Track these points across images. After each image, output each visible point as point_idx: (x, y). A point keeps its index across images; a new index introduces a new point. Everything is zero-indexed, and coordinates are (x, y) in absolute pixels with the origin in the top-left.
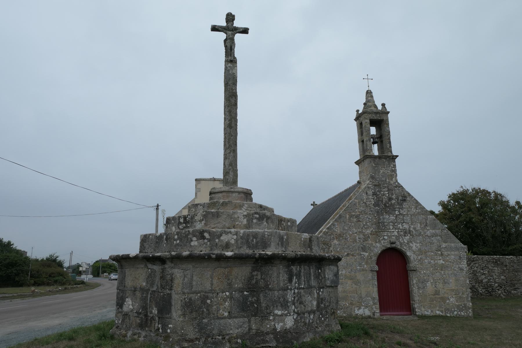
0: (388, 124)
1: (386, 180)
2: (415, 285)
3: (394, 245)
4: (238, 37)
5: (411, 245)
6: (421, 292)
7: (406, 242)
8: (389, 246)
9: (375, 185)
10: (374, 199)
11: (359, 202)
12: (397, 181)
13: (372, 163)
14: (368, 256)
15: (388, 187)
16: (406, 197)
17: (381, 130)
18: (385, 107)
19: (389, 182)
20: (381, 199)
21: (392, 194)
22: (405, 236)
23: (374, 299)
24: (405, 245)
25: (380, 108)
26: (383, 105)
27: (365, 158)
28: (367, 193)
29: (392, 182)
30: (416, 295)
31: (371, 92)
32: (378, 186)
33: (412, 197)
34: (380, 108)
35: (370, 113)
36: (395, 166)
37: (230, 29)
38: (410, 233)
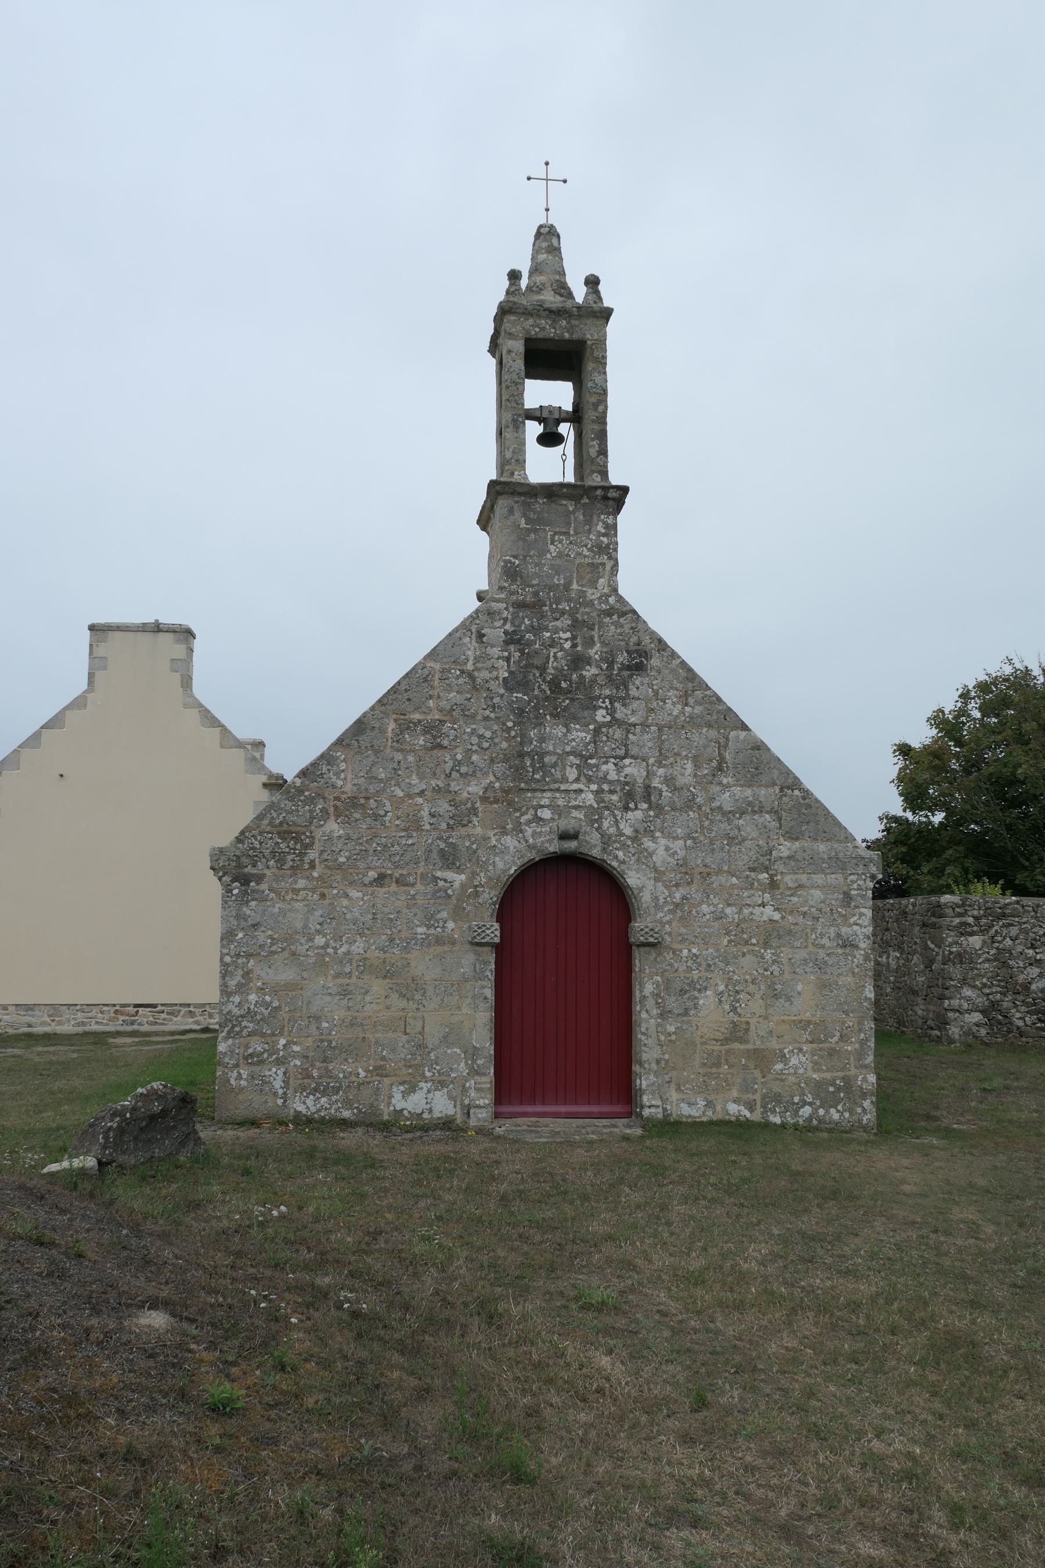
2: (650, 1003)
5: (648, 843)
6: (672, 1029)
7: (628, 831)
14: (463, 886)
22: (626, 808)
23: (472, 1053)
24: (624, 847)
30: (650, 1042)
38: (647, 798)
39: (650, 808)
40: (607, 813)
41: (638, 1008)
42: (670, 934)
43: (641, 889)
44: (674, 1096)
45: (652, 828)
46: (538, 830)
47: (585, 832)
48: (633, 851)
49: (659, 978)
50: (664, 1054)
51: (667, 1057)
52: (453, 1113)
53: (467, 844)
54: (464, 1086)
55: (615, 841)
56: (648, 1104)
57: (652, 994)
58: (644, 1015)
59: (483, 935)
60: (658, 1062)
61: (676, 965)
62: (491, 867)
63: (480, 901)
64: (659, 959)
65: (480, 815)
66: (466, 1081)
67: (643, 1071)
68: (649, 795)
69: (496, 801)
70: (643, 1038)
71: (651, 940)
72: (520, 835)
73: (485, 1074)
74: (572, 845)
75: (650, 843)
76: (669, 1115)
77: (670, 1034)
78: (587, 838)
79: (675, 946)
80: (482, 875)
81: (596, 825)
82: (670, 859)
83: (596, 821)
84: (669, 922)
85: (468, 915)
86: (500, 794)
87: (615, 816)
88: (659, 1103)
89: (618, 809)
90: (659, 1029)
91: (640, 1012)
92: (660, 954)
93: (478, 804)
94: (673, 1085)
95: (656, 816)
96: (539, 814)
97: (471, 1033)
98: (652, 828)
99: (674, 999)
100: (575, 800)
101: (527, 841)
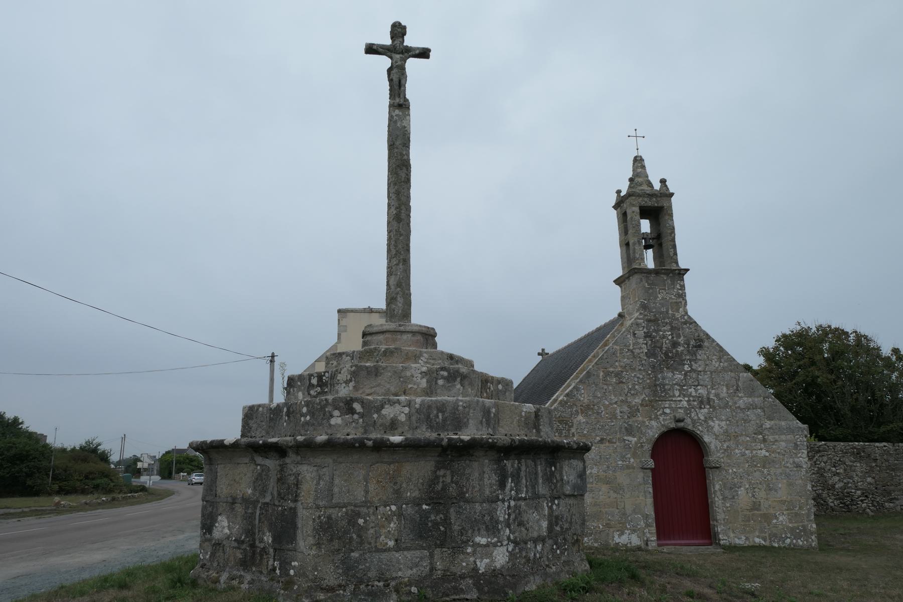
0: (671, 215)
1: (667, 312)
2: (718, 493)
3: (681, 425)
4: (412, 65)
5: (711, 423)
6: (728, 505)
7: (702, 418)
8: (673, 425)
9: (649, 321)
10: (646, 344)
11: (621, 350)
12: (686, 313)
13: (644, 281)
14: (636, 443)
15: (671, 323)
16: (702, 340)
17: (659, 224)
18: (666, 186)
19: (673, 315)
20: (658, 345)
21: (679, 336)
22: (701, 408)
23: (646, 517)
24: (701, 425)
25: (657, 186)
26: (663, 182)
27: (631, 272)
28: (634, 334)
29: (678, 315)
30: (720, 511)
31: (642, 160)
32: (654, 321)
33: (713, 341)
34: (657, 186)
35: (639, 196)
36: (683, 287)
37: (398, 50)
38: (709, 403)
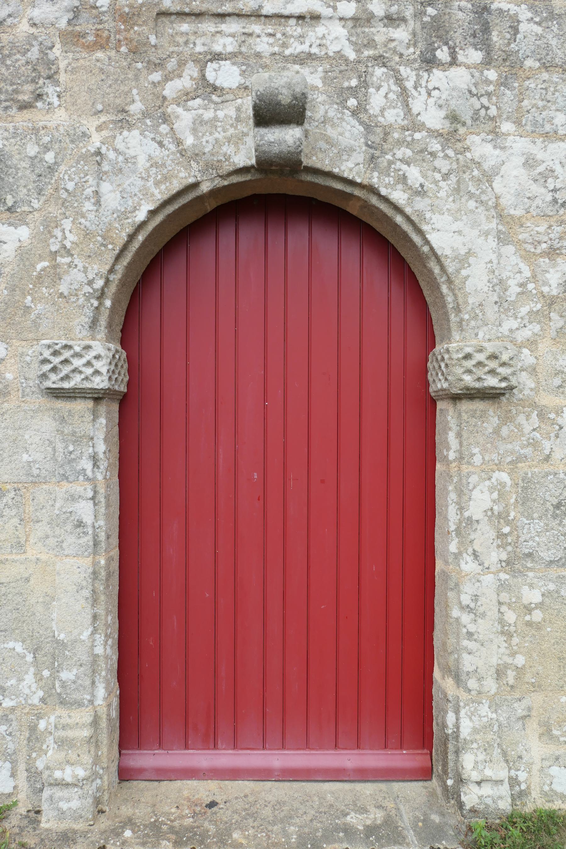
2: (484, 536)
5: (480, 147)
6: (533, 596)
7: (434, 118)
14: (24, 255)
22: (429, 62)
23: (49, 653)
24: (423, 154)
30: (484, 628)
38: (481, 35)
39: (488, 62)
40: (379, 71)
41: (453, 547)
42: (533, 371)
43: (464, 260)
44: (535, 749)
45: (493, 111)
46: (208, 115)
47: (325, 121)
48: (443, 165)
49: (504, 477)
50: (513, 654)
51: (520, 660)
52: (8, 790)
53: (32, 150)
54: (33, 728)
55: (400, 143)
56: (475, 776)
57: (490, 513)
58: (468, 565)
59: (66, 370)
60: (500, 673)
61: (547, 445)
62: (88, 206)
63: (63, 288)
64: (505, 431)
65: (62, 77)
66: (39, 717)
67: (463, 696)
68: (486, 29)
69: (101, 43)
70: (466, 618)
71: (492, 382)
72: (164, 128)
73: (79, 704)
74: (285, 137)
75: (488, 149)
76: (522, 794)
77: (528, 609)
78: (331, 132)
79: (547, 400)
80: (67, 224)
81: (352, 102)
82: (537, 189)
83: (353, 92)
84: (532, 343)
85: (36, 324)
86: (109, 24)
87: (399, 81)
88: (503, 774)
89: (409, 63)
90: (504, 597)
91: (457, 556)
92: (507, 419)
93: (57, 52)
94: (533, 726)
95: (504, 83)
96: (210, 75)
97: (47, 606)
98: (493, 111)
99: (539, 525)
100: (301, 38)
101: (179, 142)
